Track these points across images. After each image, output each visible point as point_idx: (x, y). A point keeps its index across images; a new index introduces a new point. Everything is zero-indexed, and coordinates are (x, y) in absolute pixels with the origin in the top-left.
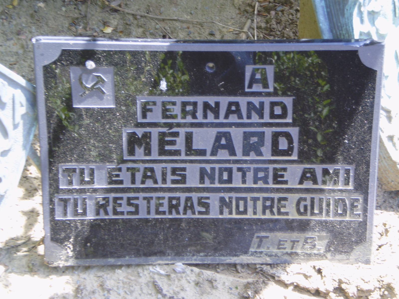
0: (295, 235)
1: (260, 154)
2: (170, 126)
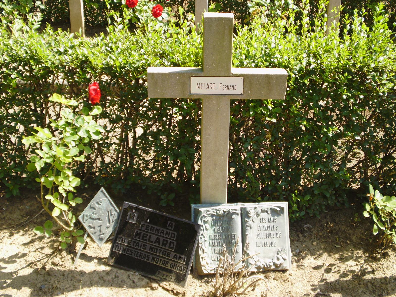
0: (168, 274)
1: (165, 247)
2: (147, 232)
